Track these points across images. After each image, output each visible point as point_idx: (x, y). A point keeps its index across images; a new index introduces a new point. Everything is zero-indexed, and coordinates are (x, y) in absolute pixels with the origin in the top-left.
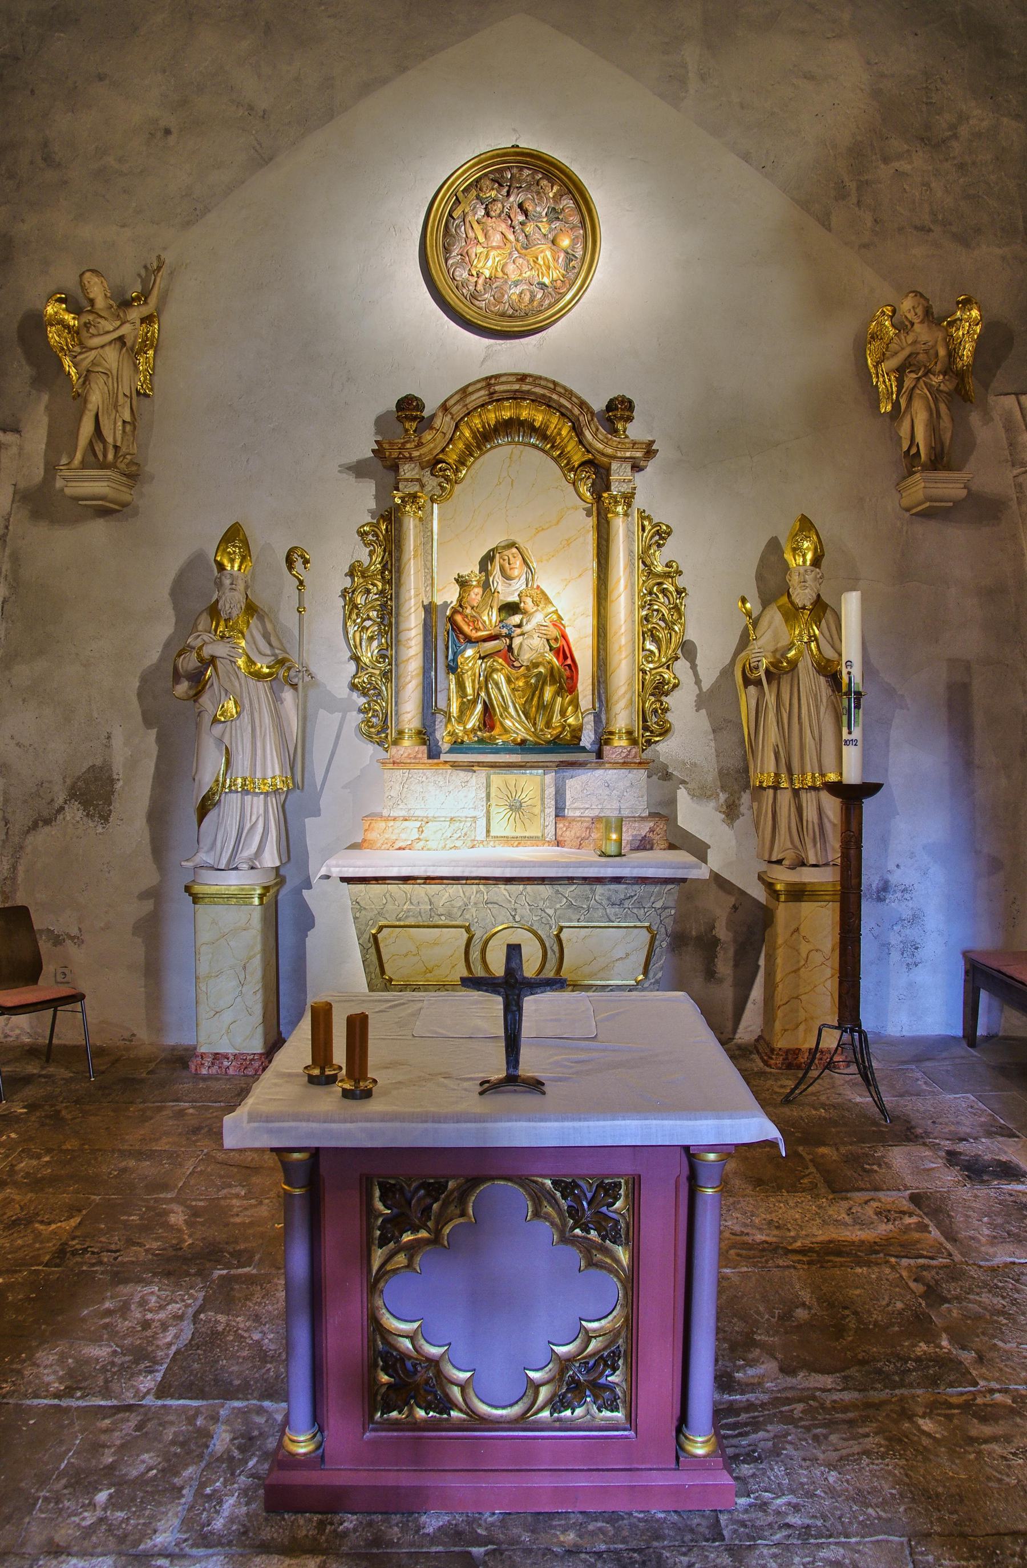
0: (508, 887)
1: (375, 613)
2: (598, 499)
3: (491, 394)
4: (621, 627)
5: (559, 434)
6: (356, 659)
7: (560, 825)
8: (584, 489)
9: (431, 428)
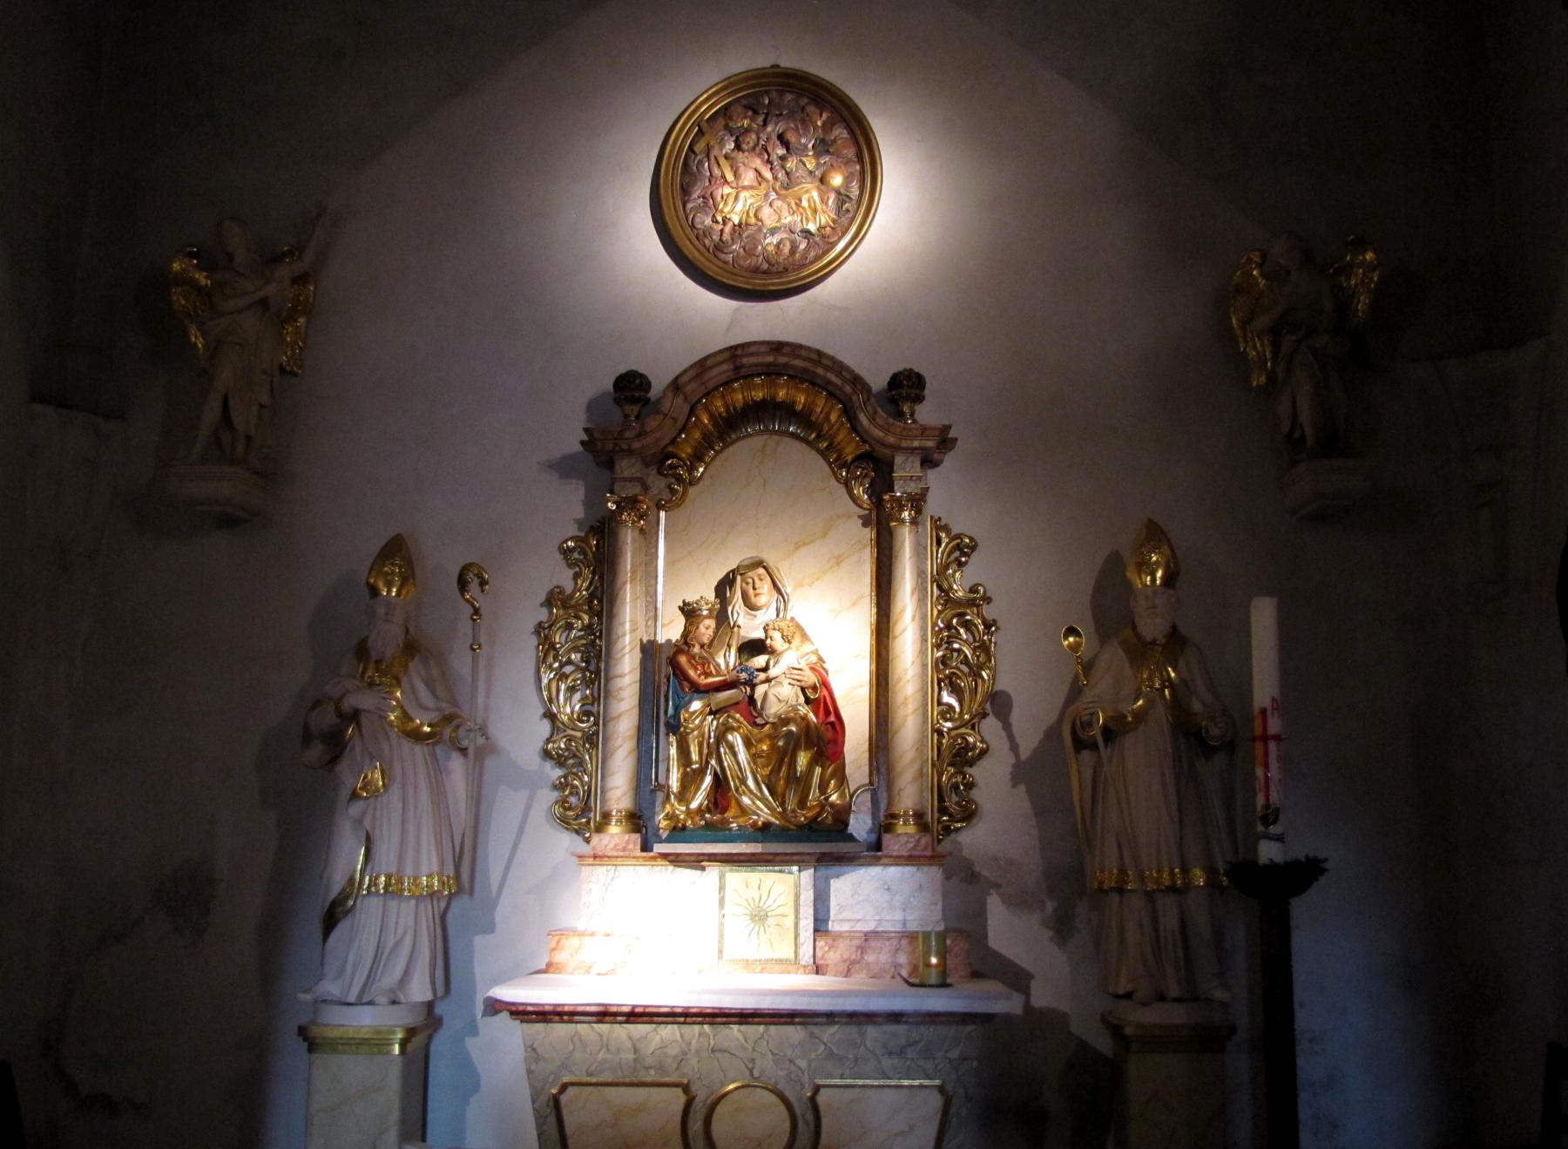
0: (743, 1028)
1: (579, 655)
2: (878, 503)
3: (737, 369)
4: (906, 671)
5: (827, 418)
6: (551, 716)
7: (820, 943)
8: (859, 491)
9: (658, 412)
